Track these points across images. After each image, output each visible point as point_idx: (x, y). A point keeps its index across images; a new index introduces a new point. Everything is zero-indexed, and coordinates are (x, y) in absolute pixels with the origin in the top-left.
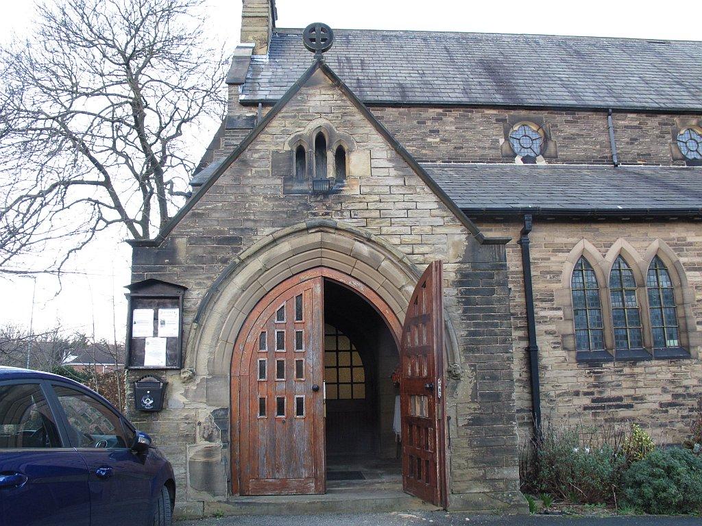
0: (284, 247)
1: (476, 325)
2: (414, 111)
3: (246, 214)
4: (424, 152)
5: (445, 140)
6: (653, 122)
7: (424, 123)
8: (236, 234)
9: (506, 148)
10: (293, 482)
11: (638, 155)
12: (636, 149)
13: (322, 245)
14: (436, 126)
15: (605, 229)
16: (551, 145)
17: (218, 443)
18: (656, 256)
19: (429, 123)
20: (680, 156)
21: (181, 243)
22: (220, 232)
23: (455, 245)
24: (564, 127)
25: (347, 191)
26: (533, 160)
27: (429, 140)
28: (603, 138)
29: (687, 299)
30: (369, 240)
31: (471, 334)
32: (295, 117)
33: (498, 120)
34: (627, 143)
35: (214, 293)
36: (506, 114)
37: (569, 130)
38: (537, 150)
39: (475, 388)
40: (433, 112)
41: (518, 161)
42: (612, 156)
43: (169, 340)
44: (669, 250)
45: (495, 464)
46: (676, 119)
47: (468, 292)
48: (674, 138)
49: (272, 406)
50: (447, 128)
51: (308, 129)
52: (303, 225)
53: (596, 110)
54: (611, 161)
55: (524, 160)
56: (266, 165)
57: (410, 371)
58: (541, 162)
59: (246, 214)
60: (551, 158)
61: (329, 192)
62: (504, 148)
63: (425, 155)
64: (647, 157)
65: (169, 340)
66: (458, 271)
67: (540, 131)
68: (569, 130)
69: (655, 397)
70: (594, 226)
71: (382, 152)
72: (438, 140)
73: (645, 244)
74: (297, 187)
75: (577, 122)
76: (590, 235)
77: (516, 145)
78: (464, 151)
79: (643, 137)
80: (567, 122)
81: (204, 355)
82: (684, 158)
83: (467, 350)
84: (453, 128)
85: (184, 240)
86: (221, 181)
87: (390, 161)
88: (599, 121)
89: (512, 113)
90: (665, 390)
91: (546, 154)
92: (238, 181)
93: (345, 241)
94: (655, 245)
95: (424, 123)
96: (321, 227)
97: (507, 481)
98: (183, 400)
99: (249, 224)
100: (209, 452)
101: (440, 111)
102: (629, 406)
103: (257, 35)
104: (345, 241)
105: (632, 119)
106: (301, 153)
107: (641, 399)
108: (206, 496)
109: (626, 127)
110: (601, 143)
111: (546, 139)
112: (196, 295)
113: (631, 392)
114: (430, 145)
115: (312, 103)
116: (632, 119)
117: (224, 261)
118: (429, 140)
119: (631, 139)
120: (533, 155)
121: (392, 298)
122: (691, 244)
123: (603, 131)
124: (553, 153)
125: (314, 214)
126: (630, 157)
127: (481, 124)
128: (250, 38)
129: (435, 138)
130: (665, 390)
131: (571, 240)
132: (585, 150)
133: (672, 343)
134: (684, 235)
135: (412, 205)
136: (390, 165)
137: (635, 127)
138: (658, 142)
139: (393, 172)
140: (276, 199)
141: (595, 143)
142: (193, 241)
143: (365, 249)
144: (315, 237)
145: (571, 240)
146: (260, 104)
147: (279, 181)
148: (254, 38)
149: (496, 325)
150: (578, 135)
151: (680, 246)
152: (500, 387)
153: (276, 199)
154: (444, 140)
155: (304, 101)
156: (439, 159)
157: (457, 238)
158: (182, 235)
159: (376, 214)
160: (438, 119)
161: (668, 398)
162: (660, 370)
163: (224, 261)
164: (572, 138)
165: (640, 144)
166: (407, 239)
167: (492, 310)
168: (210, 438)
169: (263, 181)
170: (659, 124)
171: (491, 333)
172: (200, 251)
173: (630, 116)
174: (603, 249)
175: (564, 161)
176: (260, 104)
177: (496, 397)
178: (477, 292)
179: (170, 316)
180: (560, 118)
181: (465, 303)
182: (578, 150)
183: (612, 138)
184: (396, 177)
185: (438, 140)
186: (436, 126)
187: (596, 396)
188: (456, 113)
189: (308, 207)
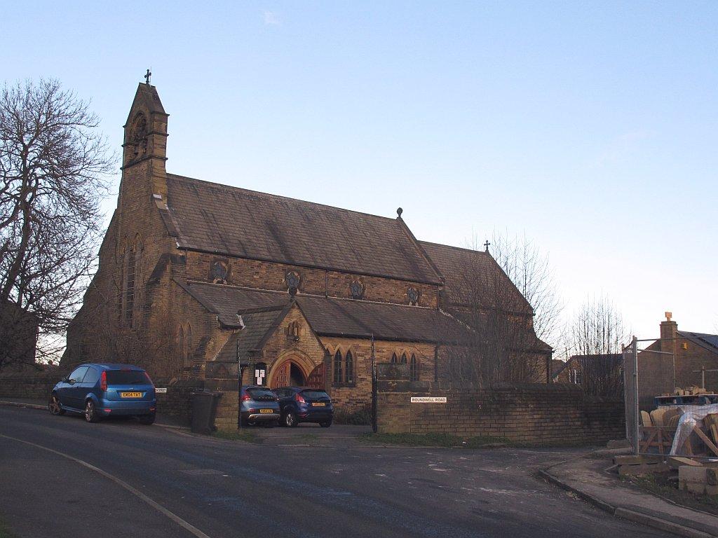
6: (343, 276)
12: (334, 289)
14: (258, 270)
15: (336, 340)
27: (255, 277)
29: (357, 366)
35: (273, 364)
37: (310, 277)
43: (263, 378)
53: (322, 268)
54: (324, 295)
56: (282, 331)
57: (134, 395)
60: (302, 291)
64: (339, 294)
65: (263, 378)
68: (310, 277)
69: (345, 400)
70: (333, 338)
71: (308, 329)
88: (322, 274)
89: (289, 266)
90: (347, 398)
102: (337, 403)
103: (163, 191)
105: (335, 274)
107: (340, 400)
112: (268, 366)
113: (337, 398)
114: (255, 280)
116: (335, 274)
118: (255, 277)
121: (308, 369)
130: (347, 398)
133: (350, 381)
151: (357, 347)
159: (456, 414)
161: (347, 400)
162: (346, 390)
173: (335, 273)
175: (306, 293)
179: (263, 371)
182: (313, 288)
186: (258, 270)
188: (267, 264)
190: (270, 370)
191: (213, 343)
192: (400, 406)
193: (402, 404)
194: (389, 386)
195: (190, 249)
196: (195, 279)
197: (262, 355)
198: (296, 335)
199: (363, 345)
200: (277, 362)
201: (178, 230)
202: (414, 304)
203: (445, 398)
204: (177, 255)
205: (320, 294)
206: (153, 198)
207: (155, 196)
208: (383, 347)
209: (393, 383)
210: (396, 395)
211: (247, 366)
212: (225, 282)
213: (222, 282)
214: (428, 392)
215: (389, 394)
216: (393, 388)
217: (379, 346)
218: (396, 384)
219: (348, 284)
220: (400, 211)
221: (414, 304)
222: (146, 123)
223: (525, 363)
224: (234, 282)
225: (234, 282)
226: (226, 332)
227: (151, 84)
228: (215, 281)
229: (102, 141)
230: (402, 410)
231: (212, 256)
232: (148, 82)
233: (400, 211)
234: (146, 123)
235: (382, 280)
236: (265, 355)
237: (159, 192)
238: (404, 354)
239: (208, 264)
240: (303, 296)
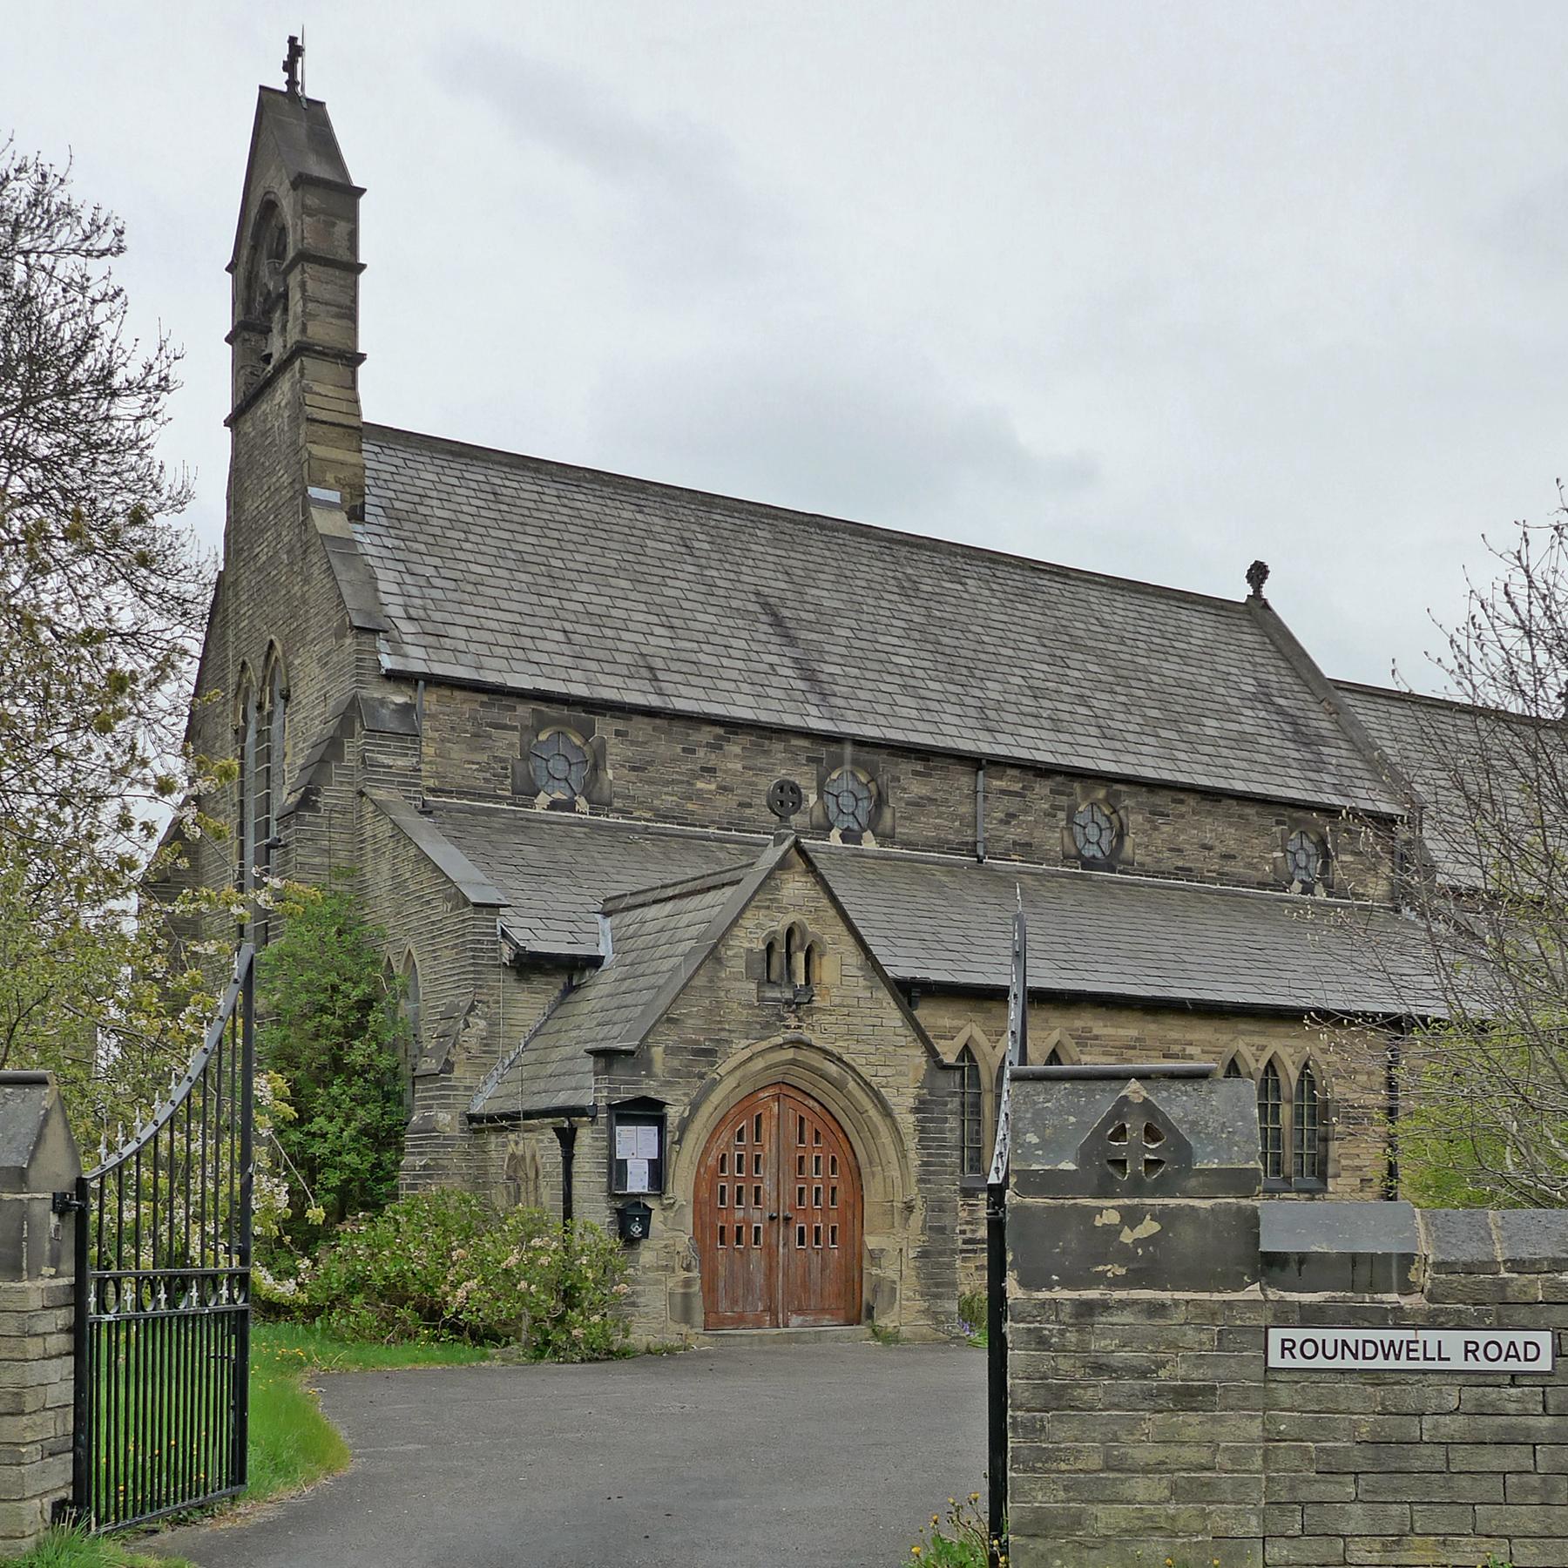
0: (759, 1064)
1: (929, 1155)
2: (678, 728)
3: (720, 1022)
4: (690, 806)
5: (725, 789)
6: (1042, 788)
7: (693, 751)
8: (708, 1045)
9: (818, 812)
10: (750, 1315)
11: (1015, 843)
12: (1013, 833)
13: (794, 1062)
14: (713, 760)
16: (887, 815)
17: (695, 1274)
18: (1054, 1051)
19: (701, 753)
20: (1073, 852)
21: (657, 1052)
22: (697, 1042)
23: (917, 1068)
24: (912, 784)
25: (818, 1002)
26: (858, 840)
27: (700, 785)
28: (964, 809)
30: (840, 1059)
31: (925, 1164)
32: (768, 908)
33: (810, 760)
34: (1001, 821)
35: (695, 1107)
36: (823, 752)
38: (863, 820)
39: (925, 1221)
40: (707, 734)
41: (835, 838)
42: (975, 843)
44: (1070, 1044)
45: (937, 1296)
46: (1077, 786)
47: (924, 1120)
48: (1070, 819)
49: (730, 1234)
50: (730, 766)
51: (780, 924)
52: (779, 1040)
54: (973, 852)
55: (844, 838)
56: (739, 966)
58: (870, 844)
59: (720, 1022)
60: (885, 838)
61: (801, 1003)
62: (815, 814)
63: (692, 813)
66: (917, 1097)
67: (872, 786)
68: (918, 788)
70: (987, 1005)
72: (713, 787)
73: (1044, 1034)
74: (769, 994)
75: (930, 776)
76: (979, 1017)
77: (833, 808)
78: (752, 811)
79: (1026, 813)
80: (916, 773)
81: (681, 1185)
82: (1079, 856)
83: (920, 1181)
84: (739, 767)
85: (660, 1049)
86: (696, 982)
87: (861, 969)
91: (880, 829)
92: (712, 985)
93: (816, 1060)
94: (1055, 1036)
95: (693, 751)
96: (797, 1044)
97: (949, 1314)
98: (661, 1227)
99: (724, 1035)
100: (687, 1283)
101: (720, 731)
104: (816, 1060)
105: (1013, 779)
106: (770, 947)
108: (684, 1329)
109: (1004, 792)
110: (962, 818)
111: (880, 801)
112: (673, 1114)
114: (699, 795)
115: (784, 892)
117: (701, 1076)
118: (700, 785)
119: (1008, 815)
120: (856, 827)
122: (1096, 1038)
123: (967, 796)
124: (888, 830)
125: (788, 1027)
126: (1000, 847)
127: (782, 763)
128: (330, 477)
129: (709, 783)
131: (956, 1023)
132: (937, 827)
134: (1090, 1024)
135: (877, 1021)
136: (860, 973)
137: (1016, 794)
138: (1046, 824)
139: (862, 982)
140: (751, 1007)
141: (954, 817)
142: (669, 1051)
143: (833, 1069)
144: (789, 1054)
145: (956, 1023)
146: (421, 683)
147: (754, 986)
148: (338, 480)
149: (946, 1156)
150: (930, 799)
152: (947, 1220)
153: (751, 1007)
154: (724, 789)
155: (777, 888)
156: (713, 822)
157: (917, 1060)
158: (658, 1043)
160: (715, 747)
163: (701, 1076)
164: (918, 804)
165: (1019, 826)
166: (872, 1059)
167: (944, 1139)
168: (688, 1269)
169: (738, 984)
170: (1052, 791)
171: (943, 1164)
172: (676, 1063)
173: (1010, 772)
174: (994, 1038)
175: (906, 844)
176: (421, 683)
177: (941, 1230)
178: (931, 1120)
180: (906, 767)
181: (921, 1132)
182: (925, 827)
183: (980, 811)
184: (866, 988)
185: (713, 787)
186: (713, 760)
187: (969, 1235)
188: (745, 739)
189: (783, 1019)
190: (684, 1125)
191: (482, 1023)
192: (1188, 1397)
193: (1198, 1376)
194: (1104, 1243)
195: (434, 681)
196: (461, 794)
197: (648, 1064)
198: (800, 980)
199: (1110, 1031)
200: (716, 1097)
201: (395, 611)
202: (1307, 889)
203: (1545, 1339)
204: (383, 702)
205: (952, 851)
206: (308, 501)
207: (314, 492)
208: (1189, 1037)
209: (1131, 1217)
210: (1156, 1310)
211: (580, 1111)
212: (582, 804)
213: (570, 806)
214: (1407, 1288)
215: (1105, 1306)
216: (1124, 1254)
217: (1174, 1035)
218: (1149, 1227)
219: (1062, 815)
220: (1258, 573)
221: (1307, 889)
222: (297, 224)
223: (539, 1233)
224: (618, 803)
225: (618, 803)
226: (538, 982)
227: (311, 92)
228: (543, 799)
229: (170, 318)
230: (1192, 1423)
231: (524, 710)
232: (292, 82)
233: (1258, 573)
234: (297, 224)
235: (1192, 801)
236: (658, 1067)
237: (330, 477)
238: (1270, 1063)
239: (514, 737)
240: (887, 858)
